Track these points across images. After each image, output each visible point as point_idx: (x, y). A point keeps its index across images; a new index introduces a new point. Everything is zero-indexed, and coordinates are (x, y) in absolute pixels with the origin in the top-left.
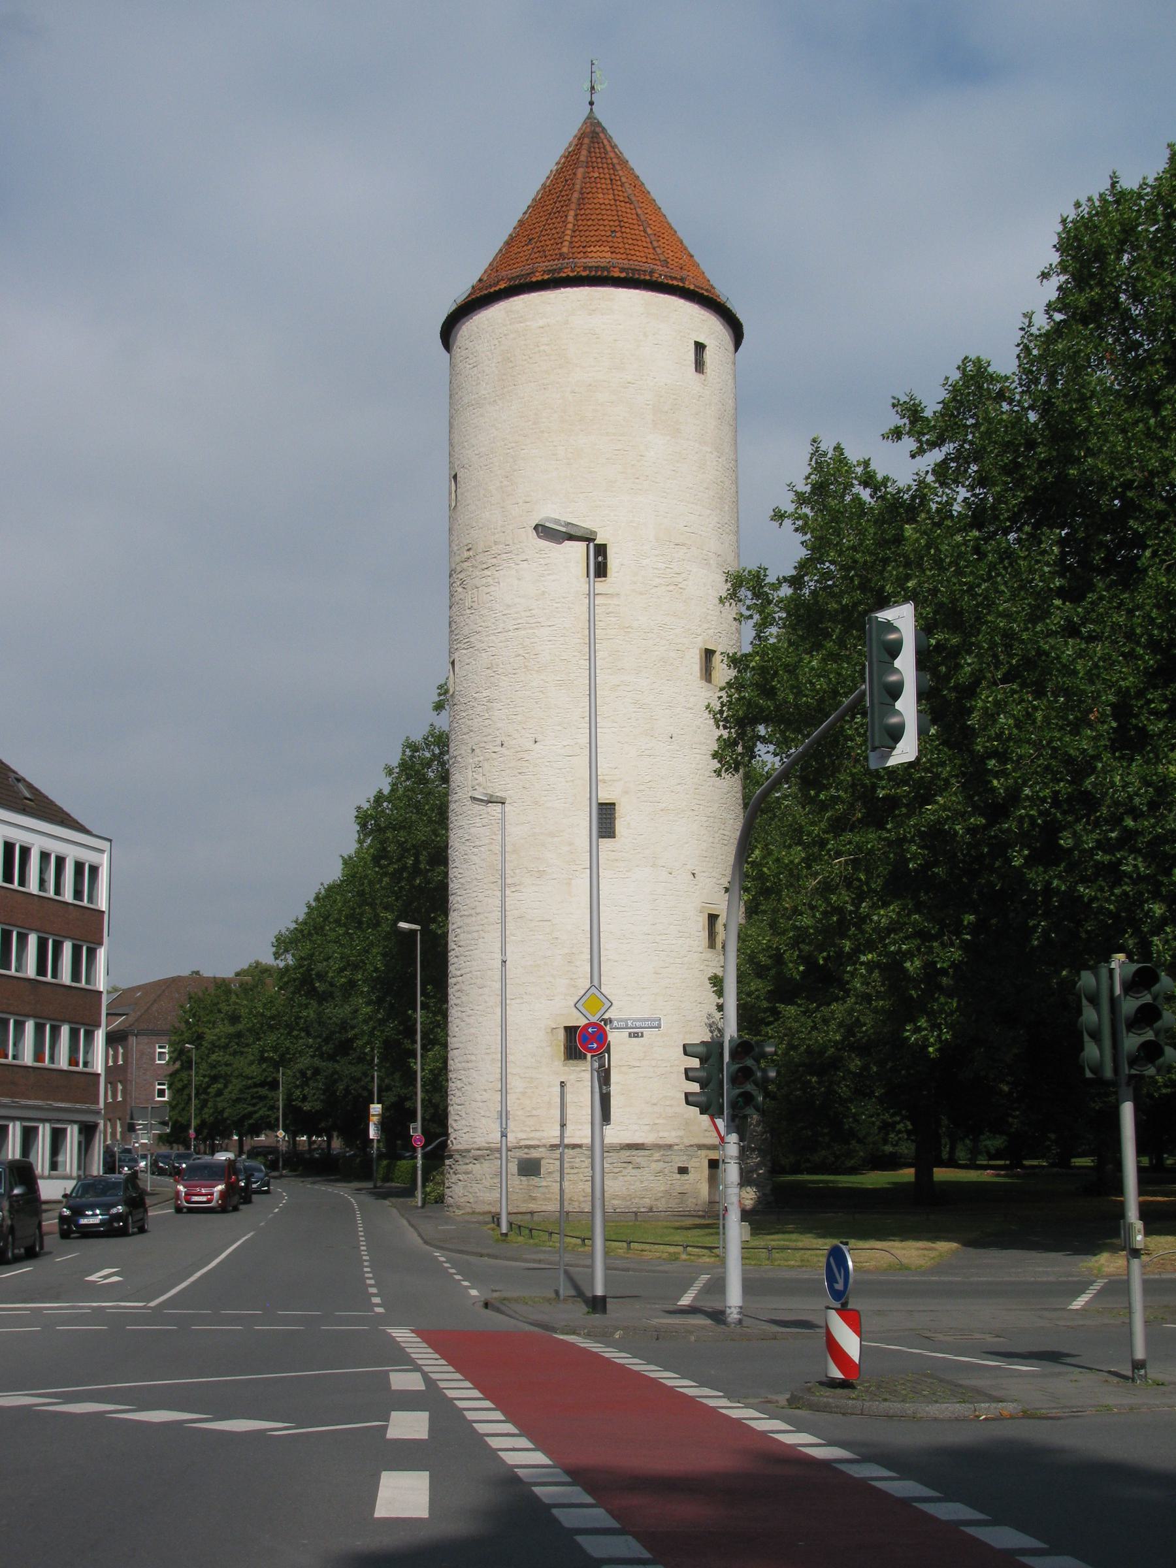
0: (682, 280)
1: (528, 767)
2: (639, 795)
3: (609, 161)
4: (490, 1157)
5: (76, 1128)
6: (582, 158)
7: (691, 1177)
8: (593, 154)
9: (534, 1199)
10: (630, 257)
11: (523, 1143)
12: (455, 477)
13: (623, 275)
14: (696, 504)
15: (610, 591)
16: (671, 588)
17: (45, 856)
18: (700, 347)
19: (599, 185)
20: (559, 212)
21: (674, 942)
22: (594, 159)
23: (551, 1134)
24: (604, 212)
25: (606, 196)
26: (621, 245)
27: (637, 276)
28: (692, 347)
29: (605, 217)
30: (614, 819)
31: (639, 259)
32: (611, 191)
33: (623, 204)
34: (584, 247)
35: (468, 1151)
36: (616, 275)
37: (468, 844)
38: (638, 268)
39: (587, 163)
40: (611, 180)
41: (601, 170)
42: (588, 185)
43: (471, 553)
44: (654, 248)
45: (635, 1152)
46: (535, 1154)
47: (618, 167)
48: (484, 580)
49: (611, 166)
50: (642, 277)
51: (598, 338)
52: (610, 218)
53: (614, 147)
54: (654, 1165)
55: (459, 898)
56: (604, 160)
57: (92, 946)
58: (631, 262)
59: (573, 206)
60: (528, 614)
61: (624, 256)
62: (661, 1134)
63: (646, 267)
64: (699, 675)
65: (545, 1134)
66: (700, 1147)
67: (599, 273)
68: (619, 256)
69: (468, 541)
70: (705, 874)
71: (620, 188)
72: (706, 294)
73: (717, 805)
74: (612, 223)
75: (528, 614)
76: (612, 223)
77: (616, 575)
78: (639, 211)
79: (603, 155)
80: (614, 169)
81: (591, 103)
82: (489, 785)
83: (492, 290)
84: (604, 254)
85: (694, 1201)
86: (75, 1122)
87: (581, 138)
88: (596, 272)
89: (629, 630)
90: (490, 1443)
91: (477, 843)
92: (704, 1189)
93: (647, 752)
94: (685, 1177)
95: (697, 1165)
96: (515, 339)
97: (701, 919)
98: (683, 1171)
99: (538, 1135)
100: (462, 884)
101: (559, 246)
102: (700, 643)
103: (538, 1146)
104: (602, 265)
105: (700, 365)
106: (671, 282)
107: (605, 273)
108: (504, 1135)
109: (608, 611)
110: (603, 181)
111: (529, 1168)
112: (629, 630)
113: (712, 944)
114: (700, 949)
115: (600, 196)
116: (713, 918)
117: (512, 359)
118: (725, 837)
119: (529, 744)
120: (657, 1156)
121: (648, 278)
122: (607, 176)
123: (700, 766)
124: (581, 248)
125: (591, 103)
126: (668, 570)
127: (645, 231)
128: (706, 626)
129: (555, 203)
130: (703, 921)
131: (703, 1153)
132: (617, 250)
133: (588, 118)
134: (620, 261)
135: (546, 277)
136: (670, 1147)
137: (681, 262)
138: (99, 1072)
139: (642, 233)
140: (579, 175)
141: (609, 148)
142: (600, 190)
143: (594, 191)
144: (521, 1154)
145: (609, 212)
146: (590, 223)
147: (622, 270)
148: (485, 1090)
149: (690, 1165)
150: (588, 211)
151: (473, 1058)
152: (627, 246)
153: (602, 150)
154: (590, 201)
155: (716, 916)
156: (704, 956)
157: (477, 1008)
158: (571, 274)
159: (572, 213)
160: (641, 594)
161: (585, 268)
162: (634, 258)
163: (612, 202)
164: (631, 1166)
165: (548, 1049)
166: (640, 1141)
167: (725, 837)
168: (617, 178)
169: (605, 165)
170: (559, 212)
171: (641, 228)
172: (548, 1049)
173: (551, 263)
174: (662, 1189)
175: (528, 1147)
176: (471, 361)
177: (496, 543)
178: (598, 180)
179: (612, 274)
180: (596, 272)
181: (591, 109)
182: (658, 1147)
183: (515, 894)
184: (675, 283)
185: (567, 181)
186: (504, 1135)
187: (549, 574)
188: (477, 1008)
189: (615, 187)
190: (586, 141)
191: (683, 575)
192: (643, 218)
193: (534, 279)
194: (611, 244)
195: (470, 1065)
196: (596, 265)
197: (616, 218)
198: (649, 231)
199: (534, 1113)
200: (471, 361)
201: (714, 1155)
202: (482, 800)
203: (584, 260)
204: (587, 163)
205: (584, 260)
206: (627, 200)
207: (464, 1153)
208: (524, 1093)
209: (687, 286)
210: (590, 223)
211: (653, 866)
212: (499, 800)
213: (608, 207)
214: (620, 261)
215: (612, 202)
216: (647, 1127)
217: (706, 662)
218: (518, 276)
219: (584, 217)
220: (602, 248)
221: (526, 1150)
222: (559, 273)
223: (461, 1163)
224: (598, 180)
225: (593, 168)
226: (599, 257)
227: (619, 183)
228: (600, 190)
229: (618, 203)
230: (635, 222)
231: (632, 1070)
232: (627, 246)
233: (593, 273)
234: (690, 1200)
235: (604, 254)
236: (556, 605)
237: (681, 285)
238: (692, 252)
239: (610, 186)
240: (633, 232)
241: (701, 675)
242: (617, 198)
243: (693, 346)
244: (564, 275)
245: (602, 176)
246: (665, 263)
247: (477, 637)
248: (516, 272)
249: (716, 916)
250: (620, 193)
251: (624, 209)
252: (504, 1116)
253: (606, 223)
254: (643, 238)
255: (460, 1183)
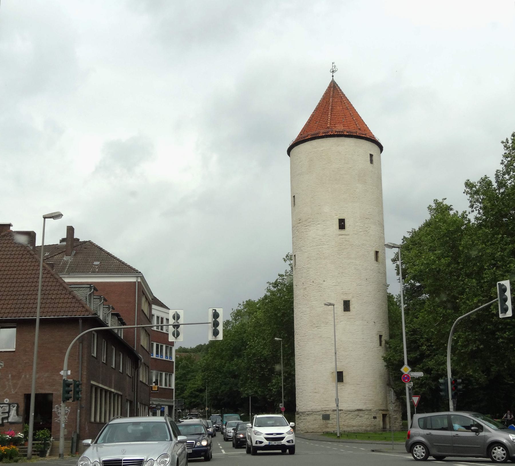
0: (365, 135)
1: (322, 289)
2: (357, 298)
3: (340, 96)
4: (313, 414)
5: (167, 407)
6: (331, 95)
7: (378, 419)
8: (335, 93)
9: (328, 427)
10: (349, 128)
11: (324, 409)
12: (294, 197)
13: (348, 134)
14: (372, 205)
15: (347, 233)
16: (365, 232)
17: (158, 317)
18: (371, 156)
19: (337, 104)
20: (325, 113)
21: (369, 344)
22: (335, 95)
23: (333, 406)
24: (340, 113)
25: (340, 107)
26: (346, 124)
27: (352, 134)
28: (369, 156)
29: (340, 114)
30: (349, 305)
31: (352, 128)
32: (341, 106)
33: (345, 110)
34: (334, 125)
35: (305, 412)
36: (346, 134)
37: (302, 313)
38: (352, 131)
39: (333, 96)
40: (341, 102)
41: (337, 99)
42: (334, 104)
43: (300, 221)
44: (356, 124)
45: (360, 412)
46: (328, 413)
47: (343, 98)
48: (305, 230)
49: (340, 97)
50: (354, 134)
51: (340, 154)
52: (342, 115)
53: (341, 90)
54: (366, 416)
55: (299, 331)
56: (338, 95)
57: (171, 346)
58: (350, 129)
59: (330, 111)
60: (320, 241)
61: (347, 127)
62: (367, 406)
63: (354, 131)
64: (374, 259)
65: (331, 406)
66: (380, 410)
67: (340, 133)
68: (346, 127)
69: (300, 217)
70: (378, 322)
71: (344, 104)
72: (373, 139)
73: (381, 300)
74: (342, 116)
75: (320, 241)
76: (342, 116)
77: (348, 228)
78: (351, 112)
79: (338, 94)
80: (342, 98)
81: (333, 76)
82: (309, 295)
83: (306, 138)
84: (341, 127)
85: (378, 427)
86: (166, 405)
87: (329, 87)
88: (339, 133)
89: (353, 246)
90: (481, 435)
91: (306, 313)
92: (381, 423)
93: (359, 284)
94: (375, 420)
95: (379, 416)
96: (313, 154)
97: (377, 337)
98: (375, 418)
99: (328, 406)
100: (301, 326)
101: (326, 124)
102: (374, 249)
103: (329, 410)
104: (341, 130)
105: (371, 161)
106: (362, 136)
107: (342, 133)
108: (337, 406)
109: (346, 240)
110: (338, 102)
111: (326, 417)
112: (353, 246)
113: (381, 345)
114: (377, 346)
115: (338, 107)
116: (381, 336)
117: (313, 160)
118: (384, 311)
119: (322, 282)
120: (367, 413)
121: (355, 134)
122: (340, 101)
123: (375, 288)
124: (334, 125)
125: (333, 76)
126: (364, 227)
127: (353, 119)
128: (375, 244)
129: (324, 110)
130: (378, 337)
131: (381, 412)
132: (345, 126)
133: (332, 81)
134: (346, 129)
135: (324, 135)
136: (370, 410)
137: (364, 128)
138: (173, 388)
139: (352, 120)
140: (331, 101)
141: (339, 91)
142: (338, 105)
143: (336, 106)
144: (323, 413)
145: (341, 113)
146: (336, 116)
147: (347, 132)
148: (310, 392)
149: (377, 416)
150: (335, 113)
151: (306, 382)
152: (348, 124)
153: (337, 92)
154: (335, 109)
155: (382, 336)
156: (379, 348)
157: (307, 366)
158: (332, 134)
159: (330, 113)
160: (356, 234)
161: (336, 132)
162: (351, 128)
163: (342, 109)
164: (359, 416)
165: (331, 379)
166: (361, 408)
167: (384, 311)
168: (343, 101)
169: (339, 97)
170: (325, 113)
171: (352, 118)
172: (331, 379)
173: (324, 130)
174: (368, 424)
175: (325, 411)
176: (299, 160)
177: (309, 218)
178: (337, 102)
179: (344, 133)
180: (339, 133)
181: (333, 78)
182: (367, 410)
183: (319, 329)
184: (364, 136)
185: (327, 102)
186: (337, 406)
187: (327, 228)
188: (307, 366)
189: (342, 104)
190: (332, 89)
191: (369, 228)
192: (352, 114)
193: (320, 135)
194: (343, 123)
195: (305, 384)
196: (339, 130)
197: (343, 114)
198: (354, 119)
199: (327, 399)
200: (299, 160)
201: (384, 413)
202: (327, 305)
203: (335, 129)
204: (333, 96)
205: (335, 129)
206: (346, 108)
207: (303, 413)
208: (323, 393)
209: (367, 137)
210: (336, 116)
211: (362, 320)
212: (333, 305)
213: (341, 111)
214: (346, 129)
215: (342, 109)
216: (363, 404)
217: (376, 255)
218: (314, 134)
219: (334, 114)
220: (340, 125)
221: (325, 412)
222: (327, 133)
223: (302, 416)
224: (337, 102)
225: (335, 98)
226: (339, 128)
227: (343, 103)
228: (338, 105)
229: (344, 110)
230: (350, 116)
231: (358, 385)
232: (348, 124)
233: (338, 133)
234: (377, 427)
235: (341, 127)
236: (330, 238)
237: (365, 136)
238: (366, 124)
239: (341, 104)
240: (349, 119)
241: (375, 259)
242: (343, 108)
243: (369, 155)
244: (329, 134)
245: (338, 100)
246: (360, 129)
247: (303, 248)
248: (313, 133)
249: (382, 336)
250: (344, 106)
251: (346, 112)
252: (337, 400)
253: (341, 116)
254: (353, 121)
255: (302, 423)
